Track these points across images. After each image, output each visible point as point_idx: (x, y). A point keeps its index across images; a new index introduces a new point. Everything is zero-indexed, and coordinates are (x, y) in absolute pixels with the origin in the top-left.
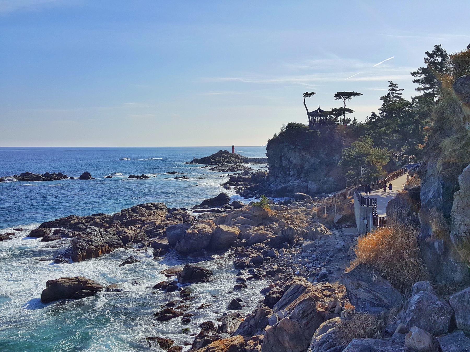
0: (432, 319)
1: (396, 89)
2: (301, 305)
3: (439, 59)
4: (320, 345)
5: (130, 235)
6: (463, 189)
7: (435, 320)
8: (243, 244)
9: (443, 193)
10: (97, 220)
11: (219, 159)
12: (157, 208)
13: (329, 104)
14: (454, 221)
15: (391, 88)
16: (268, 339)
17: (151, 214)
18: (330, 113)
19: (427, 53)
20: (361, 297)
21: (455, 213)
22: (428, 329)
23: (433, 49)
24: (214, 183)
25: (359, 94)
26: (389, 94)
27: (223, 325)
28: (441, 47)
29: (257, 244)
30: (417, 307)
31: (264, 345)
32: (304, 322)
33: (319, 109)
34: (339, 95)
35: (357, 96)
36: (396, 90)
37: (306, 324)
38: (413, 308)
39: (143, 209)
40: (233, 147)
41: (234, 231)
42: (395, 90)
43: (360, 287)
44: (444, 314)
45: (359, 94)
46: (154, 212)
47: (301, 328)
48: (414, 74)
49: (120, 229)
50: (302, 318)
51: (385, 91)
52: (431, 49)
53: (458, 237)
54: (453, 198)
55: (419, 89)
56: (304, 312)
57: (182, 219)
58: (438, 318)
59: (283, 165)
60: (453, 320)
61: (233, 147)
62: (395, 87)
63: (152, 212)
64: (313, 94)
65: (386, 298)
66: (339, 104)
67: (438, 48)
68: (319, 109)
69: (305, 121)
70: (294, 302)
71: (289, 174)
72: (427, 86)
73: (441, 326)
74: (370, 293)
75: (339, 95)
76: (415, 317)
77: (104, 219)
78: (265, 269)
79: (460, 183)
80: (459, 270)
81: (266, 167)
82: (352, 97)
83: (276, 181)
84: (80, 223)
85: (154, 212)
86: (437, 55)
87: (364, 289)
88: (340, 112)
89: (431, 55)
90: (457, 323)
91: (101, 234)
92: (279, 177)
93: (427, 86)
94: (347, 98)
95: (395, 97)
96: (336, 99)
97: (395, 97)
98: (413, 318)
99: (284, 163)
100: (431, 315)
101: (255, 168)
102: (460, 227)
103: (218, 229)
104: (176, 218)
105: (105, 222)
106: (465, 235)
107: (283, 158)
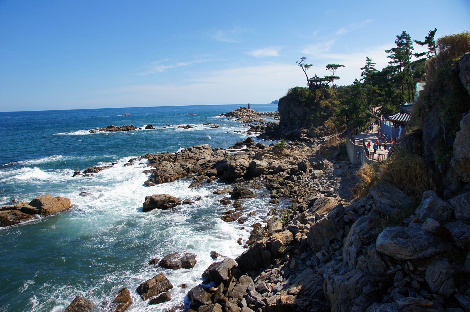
0: (439, 214)
1: (371, 62)
2: (335, 210)
3: (405, 41)
4: (359, 233)
5: (190, 167)
6: (463, 130)
7: (441, 215)
8: (270, 173)
9: (446, 132)
10: (166, 157)
11: (234, 113)
12: (204, 148)
13: (323, 73)
14: (455, 151)
15: (367, 61)
16: (312, 232)
17: (201, 153)
18: (324, 80)
19: (397, 36)
20: (383, 202)
21: (456, 146)
22: (437, 218)
23: (402, 33)
24: (242, 132)
25: (343, 66)
26: (366, 66)
27: (268, 226)
28: (406, 33)
29: (280, 173)
30: (429, 206)
31: (309, 236)
32: (336, 220)
33: (316, 76)
34: (329, 67)
35: (341, 68)
36: (371, 63)
37: (338, 222)
38: (426, 207)
39: (196, 149)
40: (249, 104)
41: (264, 164)
42: (370, 63)
43: (383, 196)
44: (447, 210)
45: (343, 66)
46: (203, 152)
47: (334, 224)
48: (388, 51)
49: (183, 163)
50: (336, 218)
51: (364, 64)
52: (400, 34)
53: (458, 162)
54: (455, 137)
55: (391, 63)
56: (337, 215)
57: (223, 156)
58: (443, 213)
59: (291, 117)
60: (453, 214)
61: (249, 104)
62: (370, 61)
63: (201, 151)
64: (388, 57)
65: (401, 202)
66: (329, 73)
67: (404, 33)
68: (316, 76)
69: (304, 85)
70: (322, 209)
71: (295, 124)
72: (397, 60)
73: (445, 218)
74: (390, 199)
75: (329, 67)
76: (427, 212)
77: (170, 156)
78: (323, 187)
79: (461, 126)
80: (454, 183)
81: (278, 119)
82: (338, 68)
83: (285, 128)
84: (155, 159)
85: (203, 152)
86: (404, 38)
87: (386, 197)
88: (331, 78)
89: (400, 38)
90: (456, 215)
91: (172, 166)
92: (287, 126)
93: (397, 60)
94: (335, 68)
95: (371, 68)
96: (327, 69)
97: (371, 68)
98: (425, 213)
99: (291, 115)
100: (438, 211)
101: (267, 120)
102: (459, 155)
103: (253, 164)
104: (219, 155)
105: (171, 158)
106: (462, 160)
107: (290, 112)
